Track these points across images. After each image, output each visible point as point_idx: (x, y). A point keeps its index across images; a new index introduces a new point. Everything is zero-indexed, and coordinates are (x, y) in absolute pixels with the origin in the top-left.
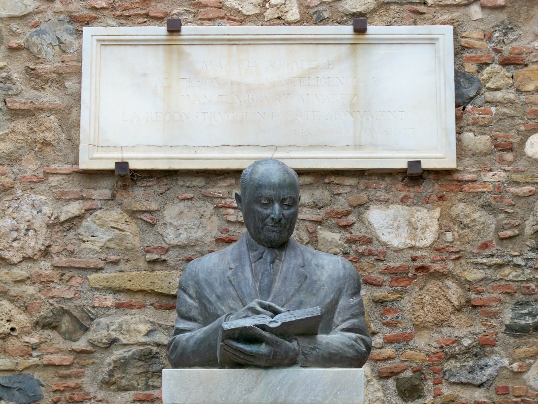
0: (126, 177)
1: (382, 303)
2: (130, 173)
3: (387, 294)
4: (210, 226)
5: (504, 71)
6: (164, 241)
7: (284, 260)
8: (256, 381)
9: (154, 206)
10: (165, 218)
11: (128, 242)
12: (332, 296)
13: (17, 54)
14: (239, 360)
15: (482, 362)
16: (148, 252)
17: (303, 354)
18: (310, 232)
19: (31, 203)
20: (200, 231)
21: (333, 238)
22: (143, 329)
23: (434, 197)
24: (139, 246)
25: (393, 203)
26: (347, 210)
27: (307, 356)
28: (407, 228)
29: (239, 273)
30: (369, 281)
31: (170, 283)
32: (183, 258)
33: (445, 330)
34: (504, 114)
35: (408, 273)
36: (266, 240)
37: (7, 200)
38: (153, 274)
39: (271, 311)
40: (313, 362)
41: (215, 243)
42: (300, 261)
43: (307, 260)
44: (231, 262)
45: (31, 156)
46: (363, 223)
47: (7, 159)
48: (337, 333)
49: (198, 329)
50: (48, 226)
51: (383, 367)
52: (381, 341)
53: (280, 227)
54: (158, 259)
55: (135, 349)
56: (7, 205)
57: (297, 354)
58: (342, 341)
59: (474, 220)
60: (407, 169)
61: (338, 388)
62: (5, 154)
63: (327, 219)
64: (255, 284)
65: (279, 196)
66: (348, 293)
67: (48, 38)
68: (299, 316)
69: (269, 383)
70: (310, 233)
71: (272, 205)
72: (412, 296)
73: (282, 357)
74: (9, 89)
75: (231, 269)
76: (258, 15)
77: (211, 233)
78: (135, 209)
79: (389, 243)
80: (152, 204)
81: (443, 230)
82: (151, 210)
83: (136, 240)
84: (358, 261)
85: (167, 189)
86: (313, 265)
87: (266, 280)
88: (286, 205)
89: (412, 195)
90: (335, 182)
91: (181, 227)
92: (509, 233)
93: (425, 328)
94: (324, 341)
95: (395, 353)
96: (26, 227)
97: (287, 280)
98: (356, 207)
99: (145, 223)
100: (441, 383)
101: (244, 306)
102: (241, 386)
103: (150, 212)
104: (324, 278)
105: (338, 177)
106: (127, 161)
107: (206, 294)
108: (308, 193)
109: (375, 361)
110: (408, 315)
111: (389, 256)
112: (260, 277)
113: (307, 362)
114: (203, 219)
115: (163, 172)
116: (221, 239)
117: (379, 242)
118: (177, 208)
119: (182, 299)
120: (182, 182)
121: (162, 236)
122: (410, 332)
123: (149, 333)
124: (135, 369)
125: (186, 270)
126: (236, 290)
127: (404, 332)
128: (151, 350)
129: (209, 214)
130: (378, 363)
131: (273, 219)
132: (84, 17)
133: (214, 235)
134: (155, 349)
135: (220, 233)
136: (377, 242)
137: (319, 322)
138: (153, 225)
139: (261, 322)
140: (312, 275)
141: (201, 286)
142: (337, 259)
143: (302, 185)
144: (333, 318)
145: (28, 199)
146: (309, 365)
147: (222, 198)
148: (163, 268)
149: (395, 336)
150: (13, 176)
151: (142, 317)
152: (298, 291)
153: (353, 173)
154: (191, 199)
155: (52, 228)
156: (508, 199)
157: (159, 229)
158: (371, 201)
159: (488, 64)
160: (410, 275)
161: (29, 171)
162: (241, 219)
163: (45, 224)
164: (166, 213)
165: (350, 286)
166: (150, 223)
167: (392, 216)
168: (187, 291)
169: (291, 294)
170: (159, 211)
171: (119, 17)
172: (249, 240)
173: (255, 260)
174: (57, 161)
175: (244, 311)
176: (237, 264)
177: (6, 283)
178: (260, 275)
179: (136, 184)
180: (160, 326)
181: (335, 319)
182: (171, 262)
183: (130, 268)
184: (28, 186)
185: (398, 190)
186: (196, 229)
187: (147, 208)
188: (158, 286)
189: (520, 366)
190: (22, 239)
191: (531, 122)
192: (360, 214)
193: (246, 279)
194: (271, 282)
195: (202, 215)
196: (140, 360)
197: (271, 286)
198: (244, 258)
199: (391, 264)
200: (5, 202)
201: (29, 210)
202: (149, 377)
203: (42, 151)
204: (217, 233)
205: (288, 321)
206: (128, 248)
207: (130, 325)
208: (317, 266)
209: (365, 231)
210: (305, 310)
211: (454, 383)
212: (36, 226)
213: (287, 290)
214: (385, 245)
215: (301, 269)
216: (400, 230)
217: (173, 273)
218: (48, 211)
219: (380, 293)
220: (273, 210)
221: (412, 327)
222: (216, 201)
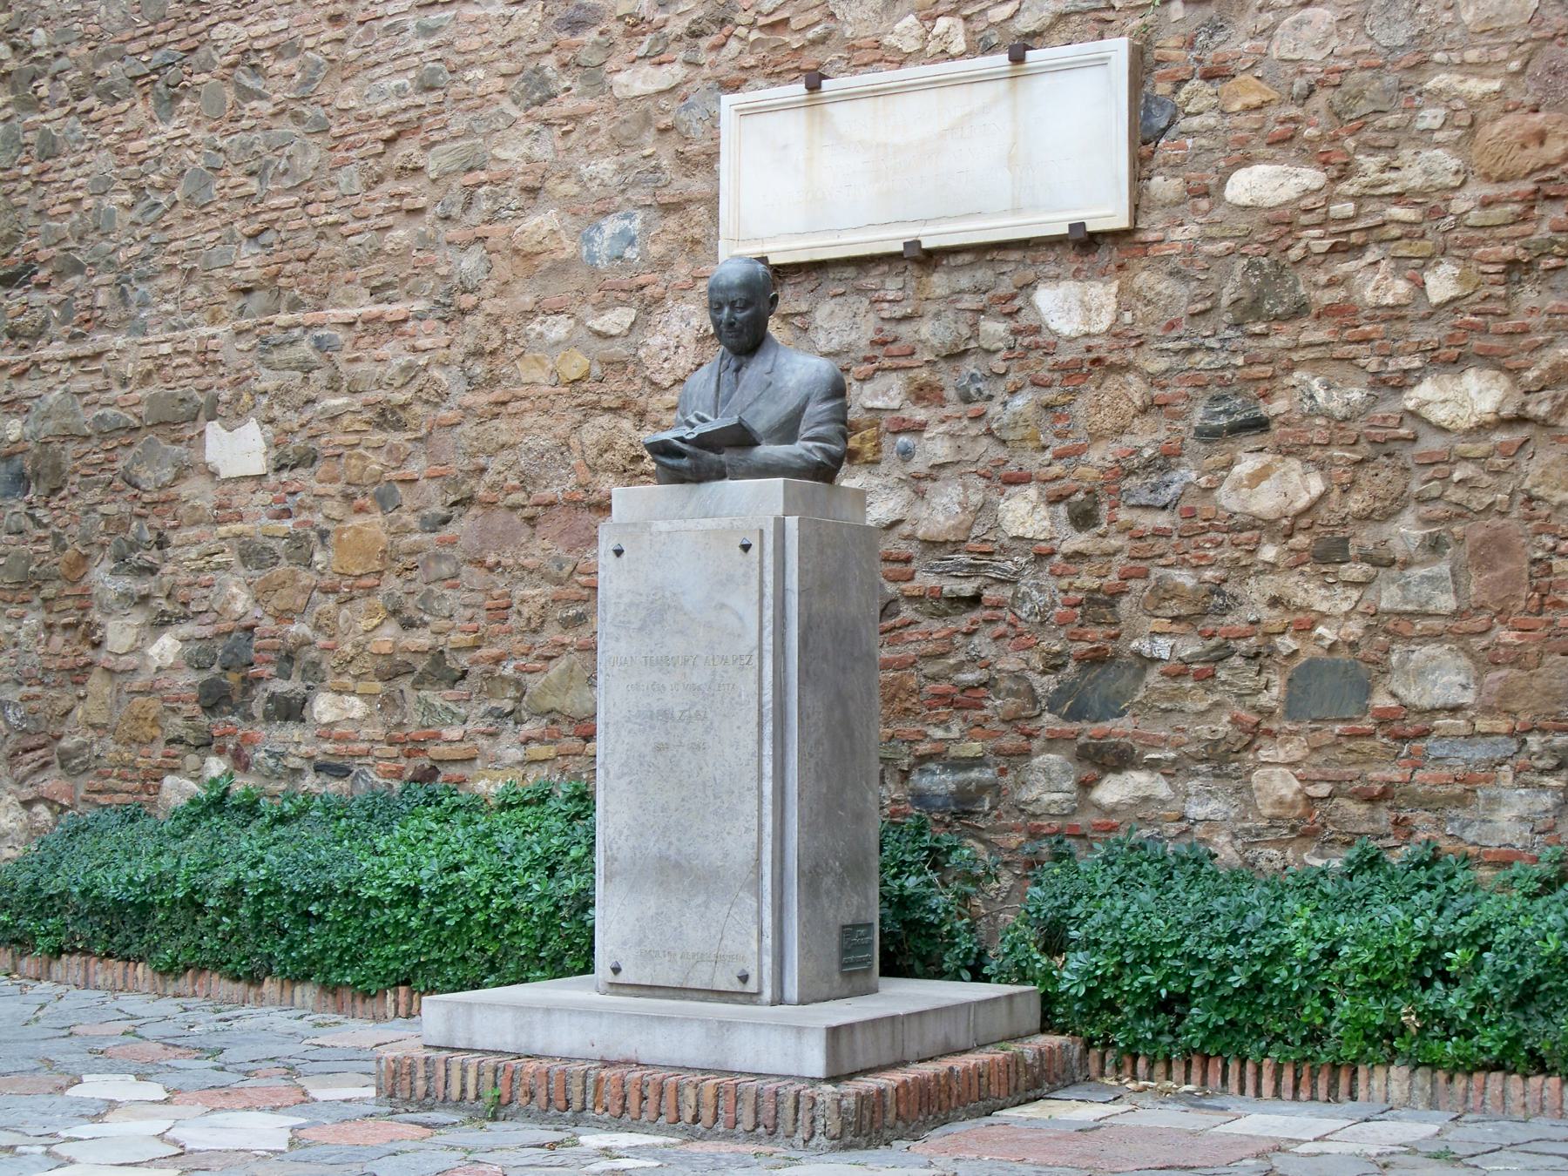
5: (1208, 89)
9: (804, 307)
13: (667, 136)
15: (1167, 478)
23: (1112, 267)
33: (1126, 439)
34: (1201, 147)
45: (681, 259)
50: (697, 341)
59: (1158, 294)
67: (697, 113)
74: (659, 179)
76: (920, 51)
81: (1122, 308)
92: (1200, 307)
93: (1102, 437)
100: (1117, 506)
104: (791, 384)
110: (1081, 423)
132: (734, 81)
152: (756, 400)
154: (843, 294)
156: (1201, 262)
159: (1186, 81)
171: (770, 75)
189: (1209, 481)
191: (1236, 155)
192: (1028, 297)
199: (1061, 359)
211: (1133, 506)
212: (684, 342)
214: (1054, 333)
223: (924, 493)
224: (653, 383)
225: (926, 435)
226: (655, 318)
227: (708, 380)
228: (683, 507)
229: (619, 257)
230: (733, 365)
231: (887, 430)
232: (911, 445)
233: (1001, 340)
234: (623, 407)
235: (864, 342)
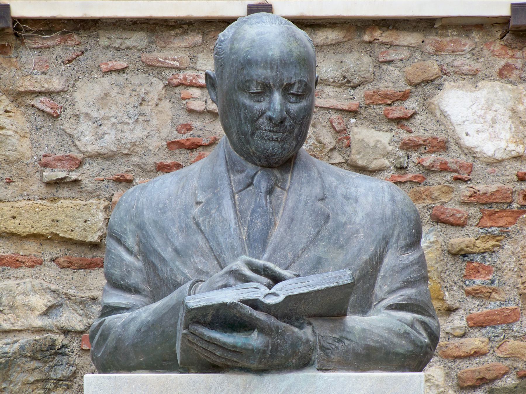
0: (7, 31)
1: (464, 256)
2: (13, 24)
3: (473, 240)
6: (76, 146)
7: (290, 188)
9: (56, 84)
10: (76, 104)
11: (10, 148)
12: (372, 250)
14: (213, 358)
16: (46, 165)
17: (322, 348)
18: (337, 129)
21: (378, 141)
22: (39, 304)
24: (30, 155)
25: (486, 77)
26: (404, 90)
27: (329, 351)
28: (510, 122)
29: (213, 211)
30: (442, 217)
31: (85, 221)
32: (109, 176)
35: (511, 203)
36: (258, 154)
38: (56, 205)
39: (267, 276)
40: (339, 362)
41: (167, 150)
42: (317, 190)
43: (330, 187)
44: (199, 191)
46: (432, 113)
48: (380, 312)
49: (144, 306)
51: (466, 369)
52: (463, 323)
53: (283, 133)
54: (65, 178)
55: (25, 339)
57: (312, 349)
58: (388, 325)
60: (510, 17)
63: (368, 106)
64: (240, 230)
70: (338, 132)
71: (268, 94)
72: (517, 244)
73: (285, 355)
75: (198, 203)
77: (159, 131)
78: (22, 89)
79: (478, 150)
80: (53, 80)
82: (52, 90)
83: (25, 145)
84: (422, 181)
85: (79, 53)
86: (340, 197)
87: (259, 224)
88: (292, 94)
89: (519, 63)
90: (381, 39)
91: (106, 122)
94: (358, 327)
95: (487, 344)
97: (294, 222)
98: (419, 84)
99: (41, 114)
101: (222, 268)
103: (49, 94)
105: (387, 30)
107: (156, 246)
108: (333, 60)
109: (451, 359)
111: (477, 173)
112: (249, 218)
113: (328, 362)
114: (146, 107)
115: (72, 22)
116: (178, 142)
117: (460, 147)
119: (115, 255)
120: (107, 40)
121: (71, 136)
122: (514, 307)
123: (48, 311)
124: (24, 374)
125: (121, 205)
126: (208, 240)
127: (504, 307)
128: (54, 341)
129: (156, 97)
130: (458, 361)
131: (270, 119)
133: (164, 135)
134: (60, 339)
135: (176, 132)
136: (457, 148)
137: (349, 294)
138: (55, 117)
139: (251, 295)
140: (337, 214)
141: (147, 232)
142: (381, 185)
143: (322, 46)
144: (374, 286)
146: (333, 366)
147: (179, 69)
148: (74, 194)
149: (487, 314)
151: (36, 282)
152: (313, 241)
153: (414, 24)
154: (123, 70)
158: (445, 74)
160: (515, 206)
162: (213, 107)
164: (78, 96)
165: (402, 232)
166: (49, 114)
167: (483, 101)
168: (123, 240)
169: (302, 246)
170: (65, 92)
172: (230, 153)
173: (240, 188)
175: (222, 276)
176: (209, 196)
178: (249, 213)
179: (23, 43)
180: (69, 299)
181: (377, 288)
182: (88, 183)
183: (14, 195)
185: (494, 55)
186: (132, 125)
188: (66, 227)
193: (225, 221)
194: (268, 226)
195: (143, 100)
196: (34, 358)
197: (268, 232)
198: (221, 185)
199: (482, 188)
202: (49, 389)
204: (171, 133)
205: (296, 293)
206: (11, 158)
207: (15, 297)
208: (347, 197)
209: (435, 128)
210: (325, 275)
214: (471, 152)
215: (320, 204)
216: (497, 126)
217: (91, 203)
219: (462, 239)
220: (270, 103)
221: (518, 298)
222: (168, 74)
233: (387, 155)
235: (154, 143)
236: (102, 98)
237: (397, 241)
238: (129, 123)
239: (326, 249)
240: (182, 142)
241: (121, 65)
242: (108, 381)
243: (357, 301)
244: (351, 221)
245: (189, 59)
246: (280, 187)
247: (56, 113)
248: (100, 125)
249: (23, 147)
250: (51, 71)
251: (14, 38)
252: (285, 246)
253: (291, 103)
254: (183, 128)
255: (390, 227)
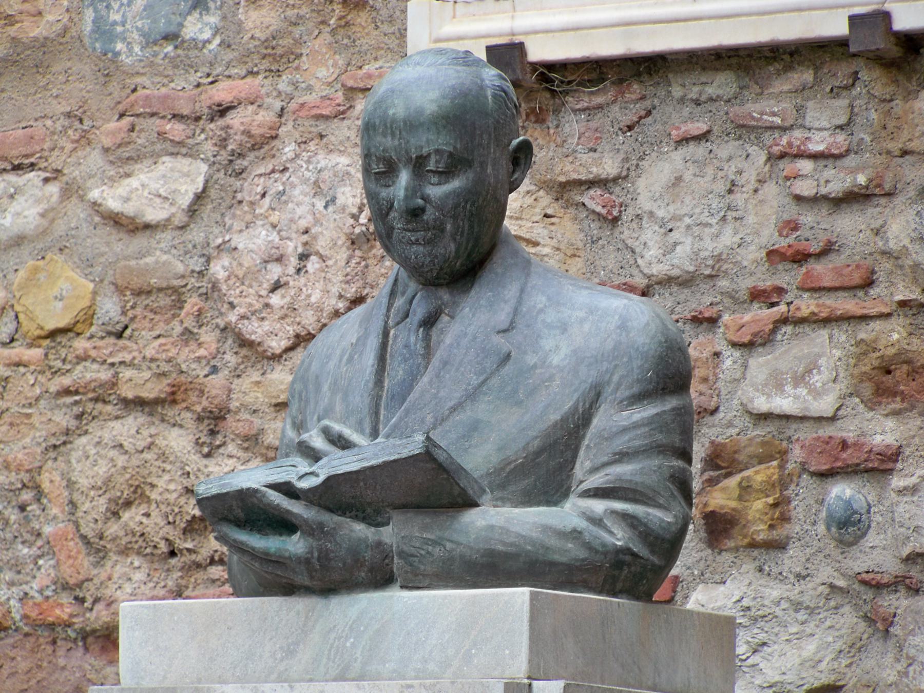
4: (756, 214)
8: (304, 625)
9: (609, 167)
19: (313, 179)
20: (728, 230)
27: (415, 559)
37: (261, 175)
45: (320, 43)
47: (264, 57)
56: (259, 189)
61: (472, 637)
62: (257, 43)
65: (407, 152)
66: (618, 395)
68: (371, 459)
69: (330, 631)
78: (562, 179)
82: (603, 176)
91: (678, 224)
96: (300, 250)
97: (448, 367)
99: (596, 218)
102: (275, 640)
104: (556, 360)
106: (517, 39)
113: (416, 575)
114: (739, 195)
118: (667, 165)
129: (753, 178)
133: (764, 240)
145: (307, 169)
146: (427, 582)
150: (278, 105)
152: (472, 395)
155: (365, 247)
157: (626, 233)
161: (317, 85)
163: (343, 238)
174: (382, 52)
177: (255, 411)
184: (313, 129)
187: (591, 173)
190: (291, 283)
195: (733, 184)
200: (256, 179)
201: (307, 199)
203: (347, 24)
212: (321, 245)
213: (442, 394)
218: (351, 200)
222: (768, 138)
223: (889, 621)
224: (244, 343)
225: (897, 482)
226: (252, 187)
227: (361, 341)
228: (290, 652)
229: (171, 37)
230: (419, 311)
231: (804, 468)
232: (860, 504)
234: (171, 399)
235: (752, 254)
236: (673, 184)
237: (617, 389)
238: (710, 224)
239: (492, 407)
240: (783, 250)
241: (698, 128)
242: (146, 611)
243: (535, 485)
244: (545, 362)
245: (794, 111)
246: (448, 315)
247: (611, 214)
248: (671, 230)
249: (570, 272)
250: (605, 146)
251: (548, 95)
252: (425, 405)
253: (432, 184)
254: (785, 227)
255: (607, 369)
